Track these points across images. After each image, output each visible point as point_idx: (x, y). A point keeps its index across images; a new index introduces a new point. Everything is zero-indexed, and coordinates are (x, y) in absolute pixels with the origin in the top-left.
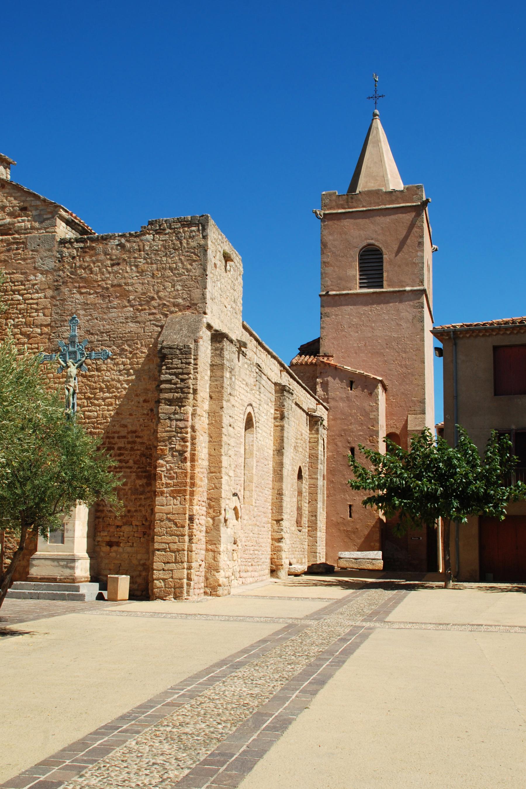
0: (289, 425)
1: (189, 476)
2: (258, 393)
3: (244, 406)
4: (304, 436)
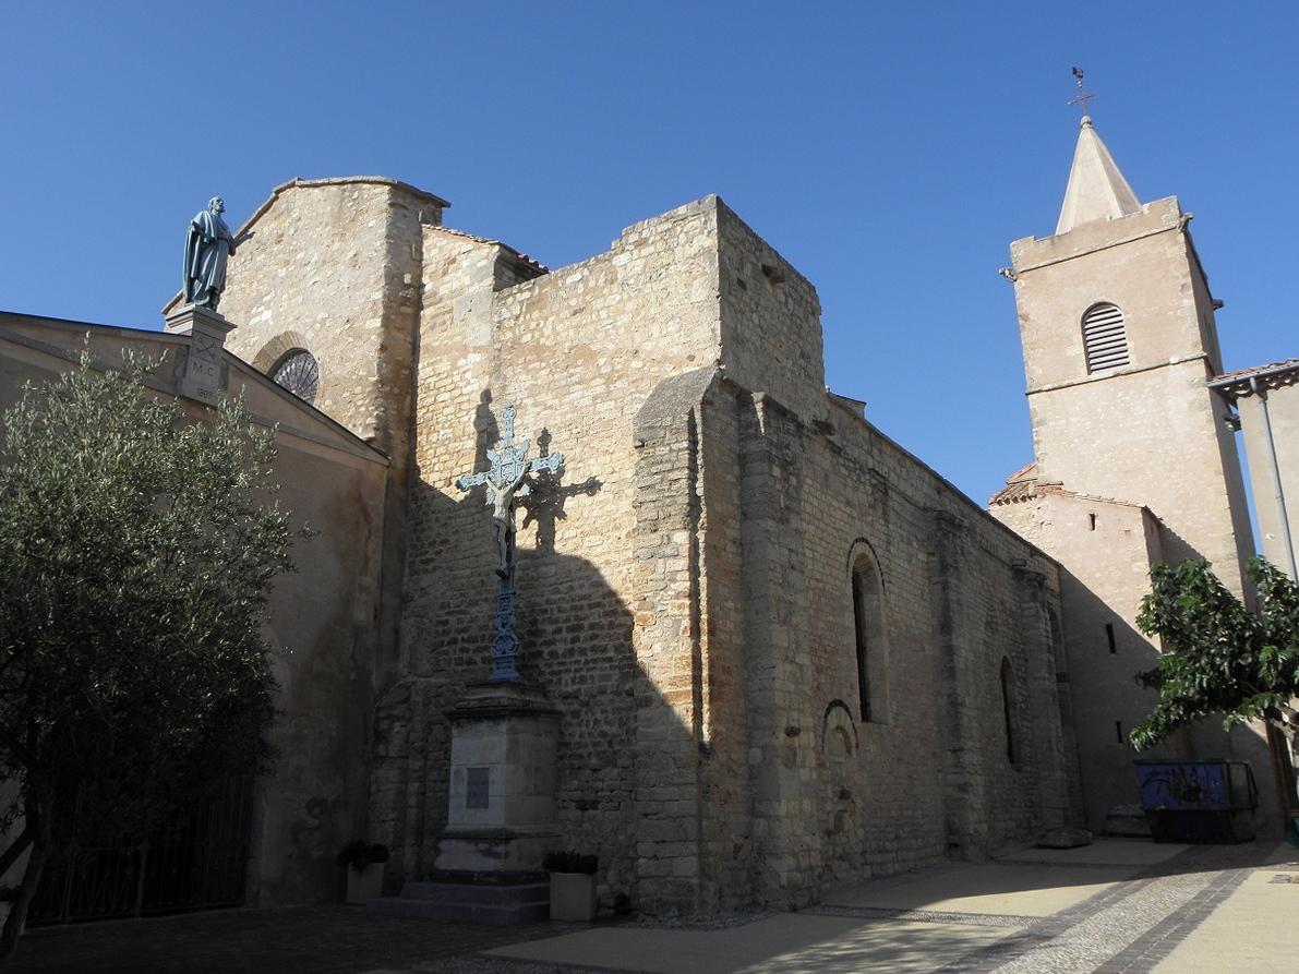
0: (960, 580)
2: (882, 522)
3: (846, 541)
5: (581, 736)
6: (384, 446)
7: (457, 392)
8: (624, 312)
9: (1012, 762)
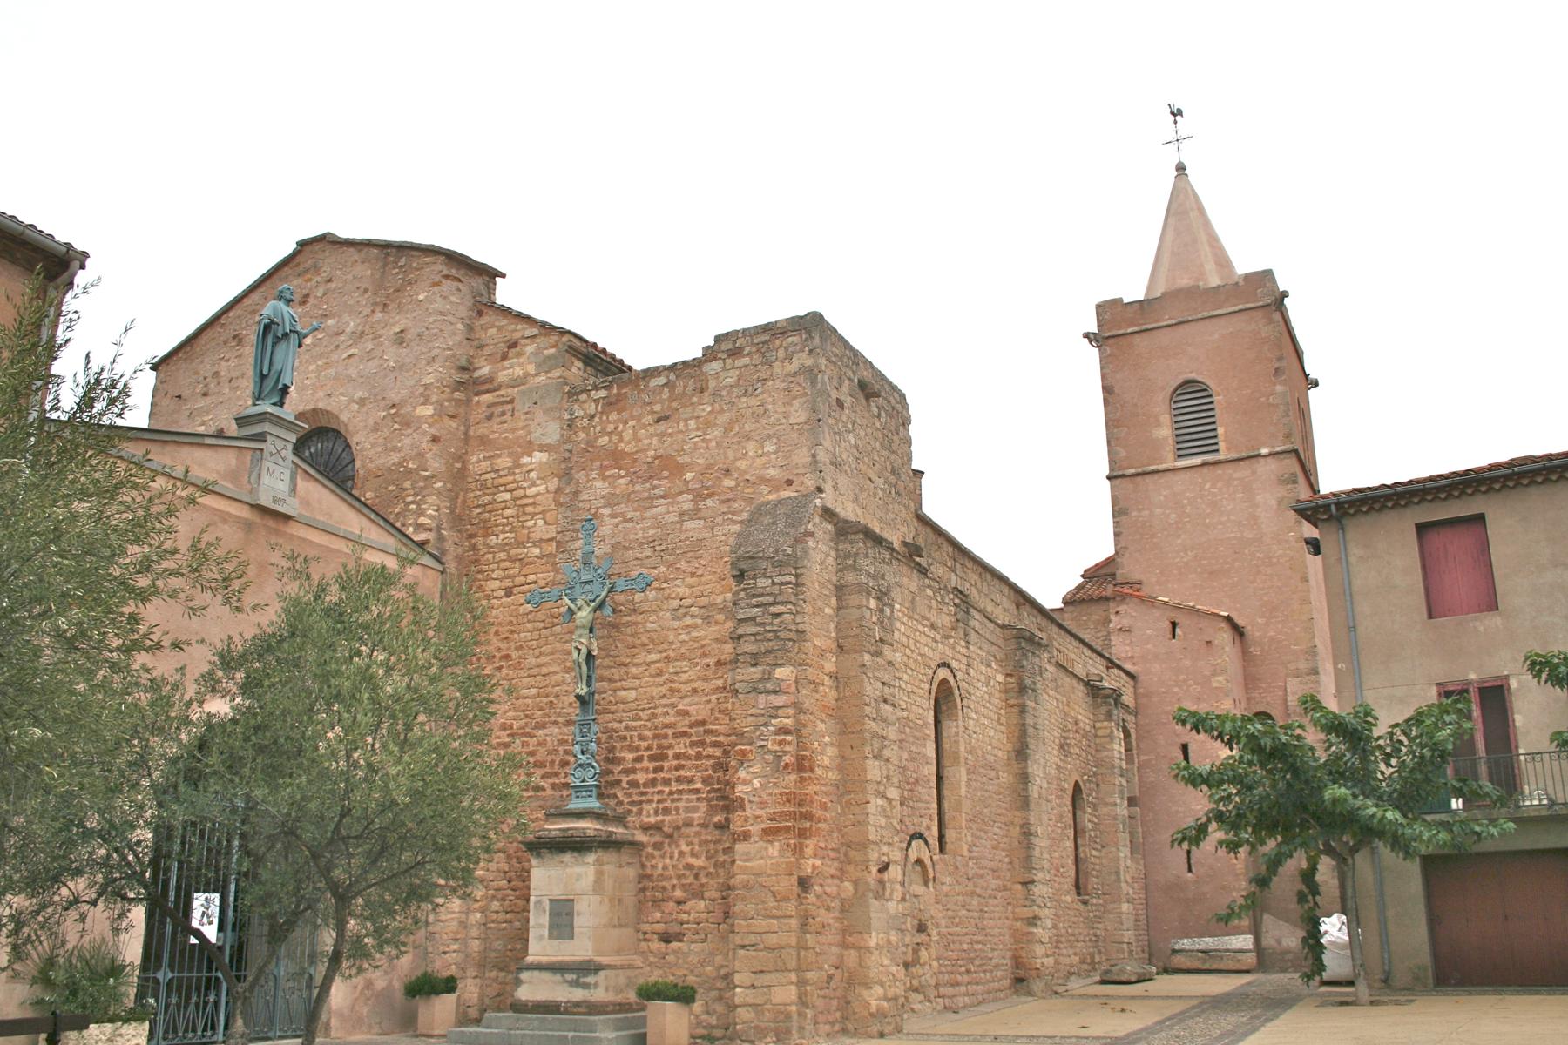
2: (963, 643)
3: (930, 667)
4: (1081, 725)
5: (665, 868)
6: (438, 549)
7: (520, 493)
8: (715, 425)
9: (1079, 894)
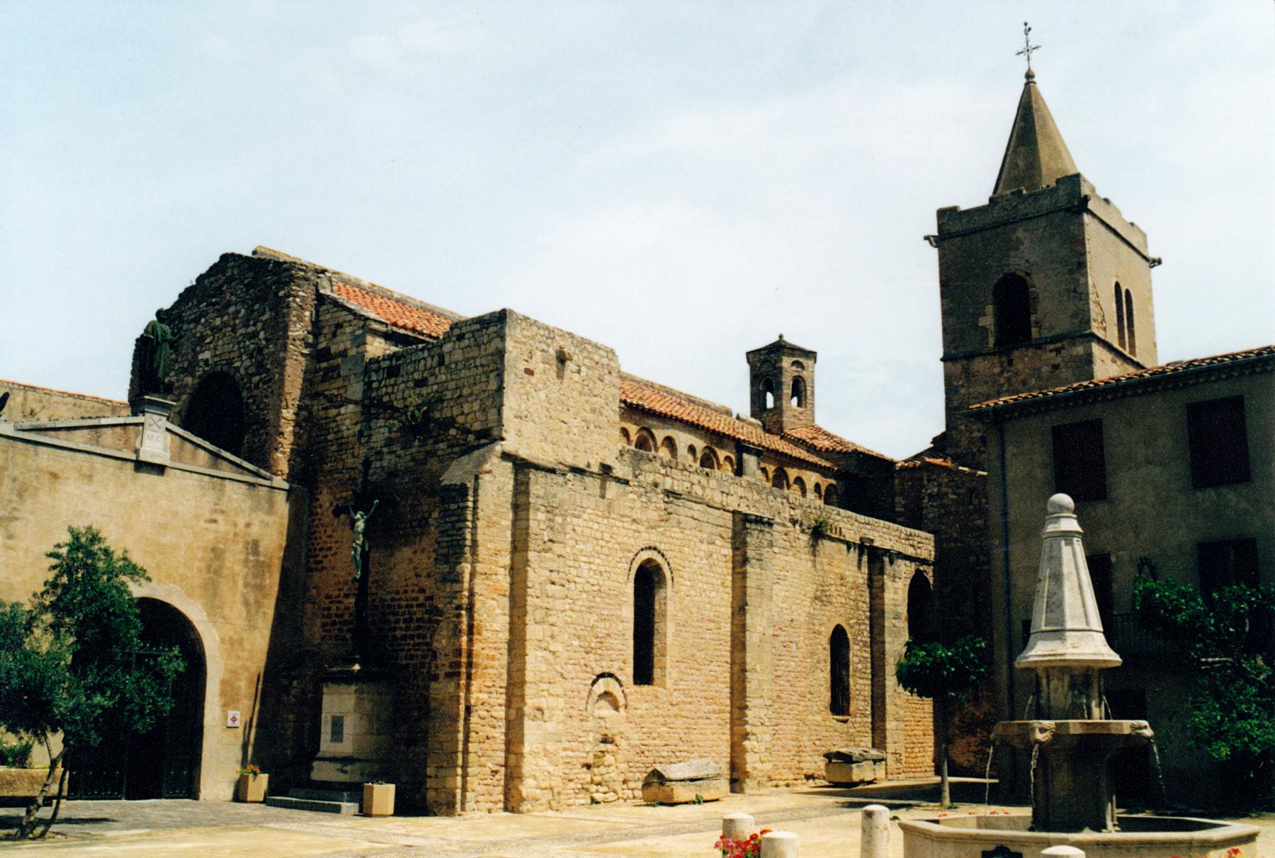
1: (464, 654)
